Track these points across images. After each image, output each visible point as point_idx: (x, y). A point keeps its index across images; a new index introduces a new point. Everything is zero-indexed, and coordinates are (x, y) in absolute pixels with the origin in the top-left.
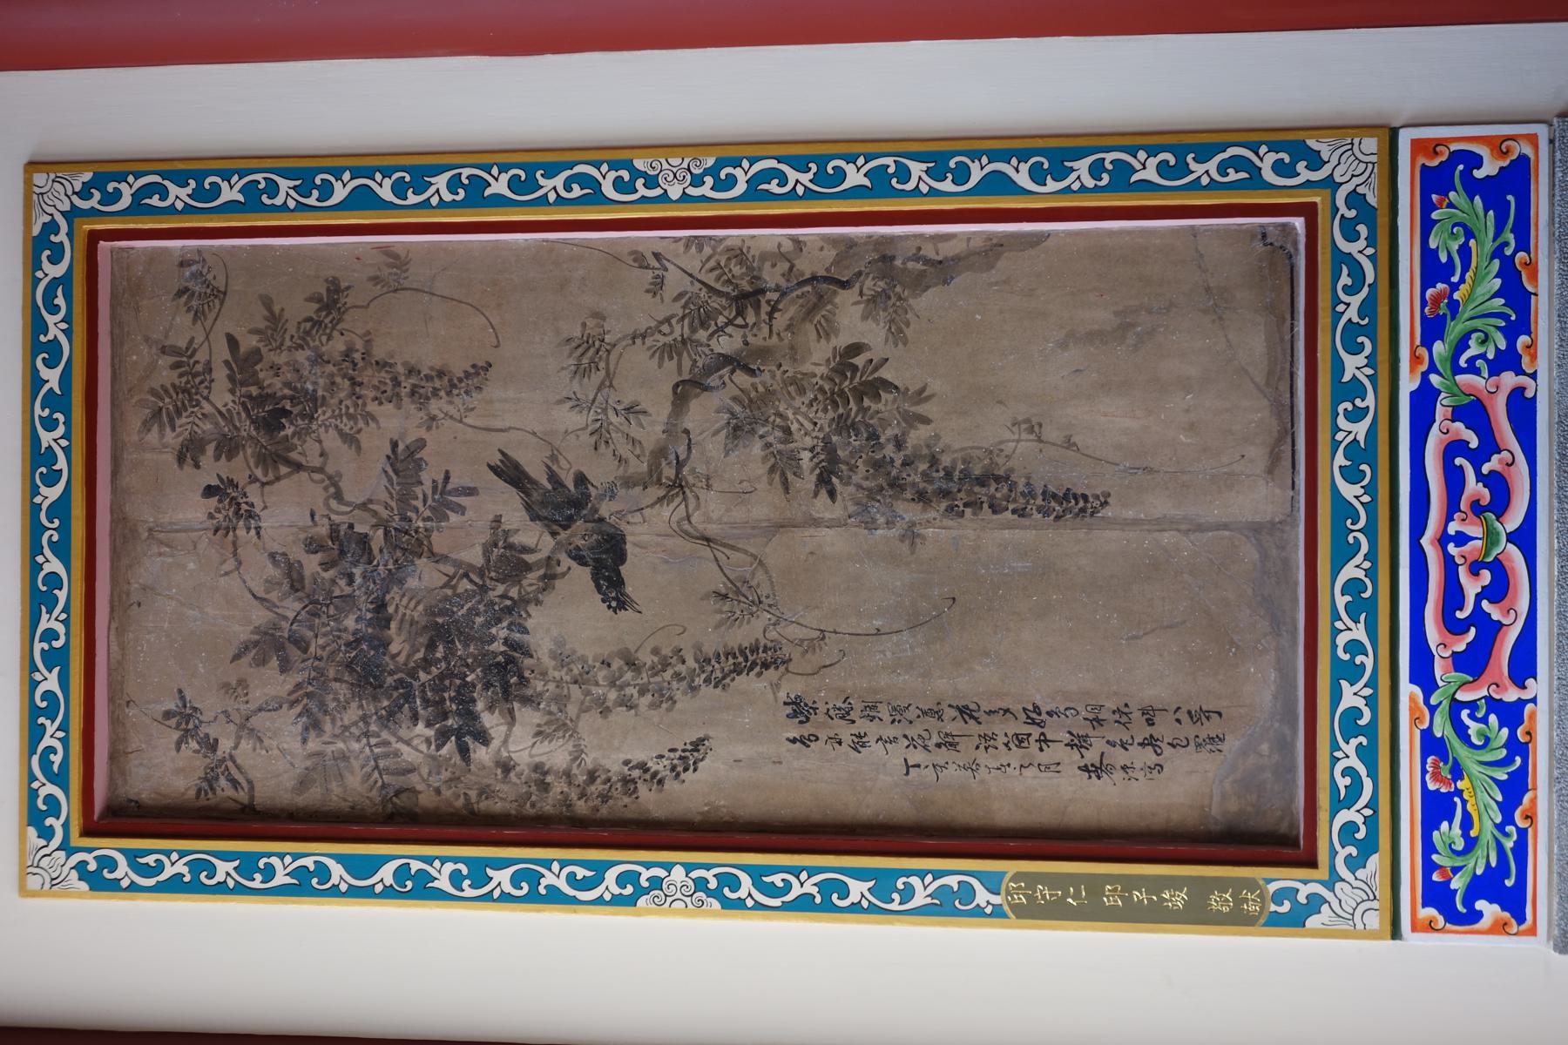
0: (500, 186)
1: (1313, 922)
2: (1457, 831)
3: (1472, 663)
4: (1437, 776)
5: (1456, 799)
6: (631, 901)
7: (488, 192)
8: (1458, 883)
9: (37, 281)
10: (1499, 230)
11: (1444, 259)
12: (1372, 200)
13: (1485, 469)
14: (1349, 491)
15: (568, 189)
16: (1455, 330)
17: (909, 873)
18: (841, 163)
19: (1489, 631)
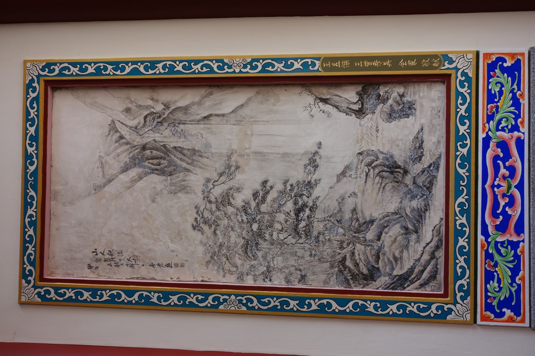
0: (293, 303)
1: (449, 317)
2: (496, 285)
3: (502, 228)
4: (489, 266)
5: (495, 273)
6: (254, 60)
7: (298, 302)
8: (495, 303)
9: (28, 98)
10: (512, 85)
11: (493, 92)
12: (470, 75)
13: (507, 164)
14: (461, 171)
15: (202, 69)
16: (497, 117)
17: (165, 73)
18: (293, 61)
19: (507, 218)
